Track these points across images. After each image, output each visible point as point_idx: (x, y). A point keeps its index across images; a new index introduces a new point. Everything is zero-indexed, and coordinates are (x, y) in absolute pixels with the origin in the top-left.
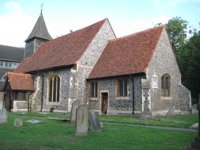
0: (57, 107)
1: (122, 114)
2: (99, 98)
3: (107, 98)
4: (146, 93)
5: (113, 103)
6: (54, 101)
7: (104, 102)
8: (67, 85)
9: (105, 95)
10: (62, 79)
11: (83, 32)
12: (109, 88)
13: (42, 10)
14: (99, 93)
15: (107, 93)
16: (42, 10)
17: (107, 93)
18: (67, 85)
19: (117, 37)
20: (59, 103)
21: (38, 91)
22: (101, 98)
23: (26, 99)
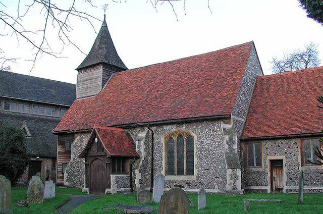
0: (188, 183)
1: (313, 191)
2: (266, 167)
3: (282, 167)
4: (231, 148)
5: (294, 175)
6: (180, 172)
7: (274, 173)
8: (210, 148)
9: (276, 164)
10: (199, 137)
11: (208, 60)
12: (286, 153)
13: (105, 15)
14: (265, 160)
15: (281, 161)
16: (105, 15)
17: (281, 161)
18: (210, 148)
19: (265, 74)
20: (193, 178)
21: (145, 158)
22: (269, 167)
23: (126, 172)
